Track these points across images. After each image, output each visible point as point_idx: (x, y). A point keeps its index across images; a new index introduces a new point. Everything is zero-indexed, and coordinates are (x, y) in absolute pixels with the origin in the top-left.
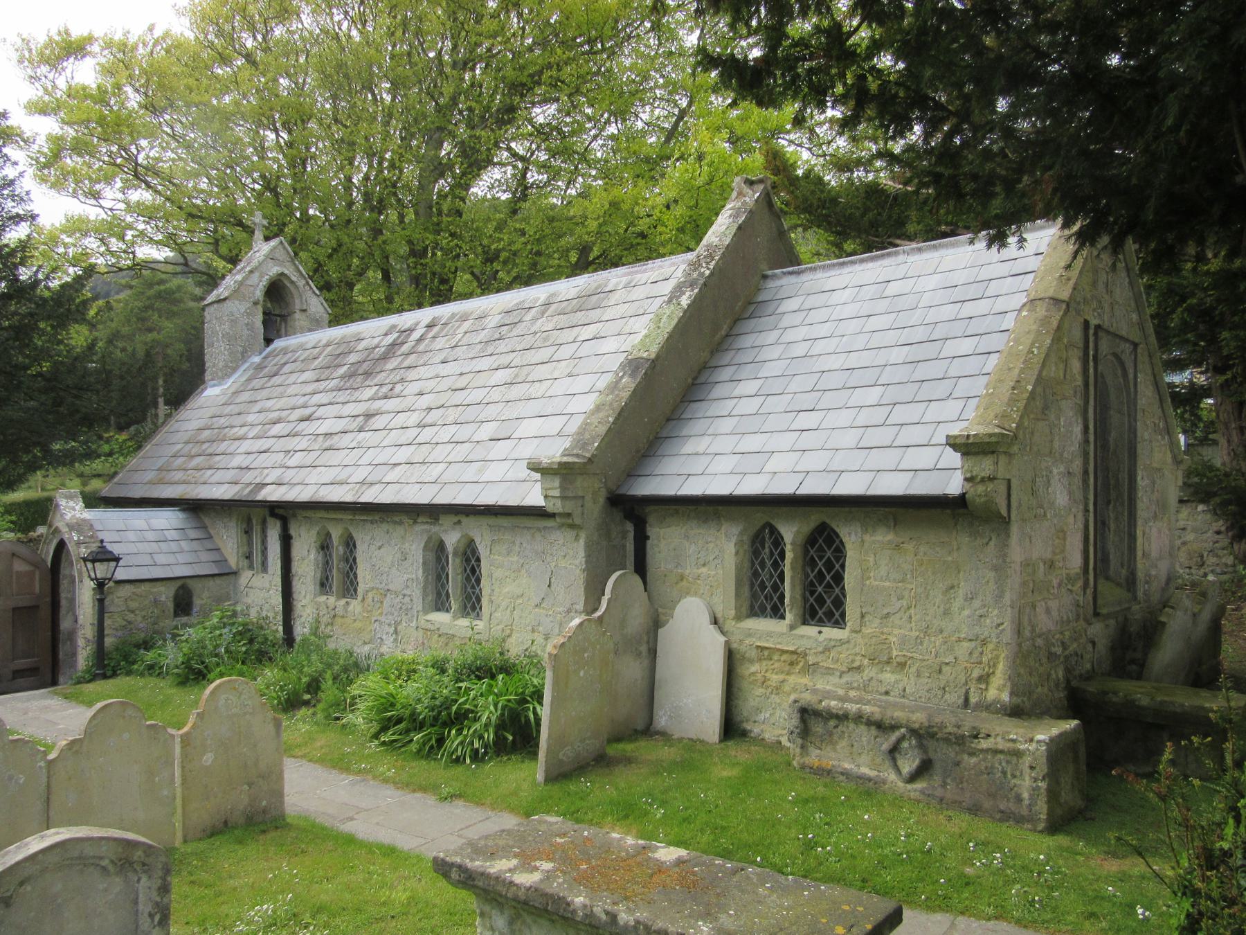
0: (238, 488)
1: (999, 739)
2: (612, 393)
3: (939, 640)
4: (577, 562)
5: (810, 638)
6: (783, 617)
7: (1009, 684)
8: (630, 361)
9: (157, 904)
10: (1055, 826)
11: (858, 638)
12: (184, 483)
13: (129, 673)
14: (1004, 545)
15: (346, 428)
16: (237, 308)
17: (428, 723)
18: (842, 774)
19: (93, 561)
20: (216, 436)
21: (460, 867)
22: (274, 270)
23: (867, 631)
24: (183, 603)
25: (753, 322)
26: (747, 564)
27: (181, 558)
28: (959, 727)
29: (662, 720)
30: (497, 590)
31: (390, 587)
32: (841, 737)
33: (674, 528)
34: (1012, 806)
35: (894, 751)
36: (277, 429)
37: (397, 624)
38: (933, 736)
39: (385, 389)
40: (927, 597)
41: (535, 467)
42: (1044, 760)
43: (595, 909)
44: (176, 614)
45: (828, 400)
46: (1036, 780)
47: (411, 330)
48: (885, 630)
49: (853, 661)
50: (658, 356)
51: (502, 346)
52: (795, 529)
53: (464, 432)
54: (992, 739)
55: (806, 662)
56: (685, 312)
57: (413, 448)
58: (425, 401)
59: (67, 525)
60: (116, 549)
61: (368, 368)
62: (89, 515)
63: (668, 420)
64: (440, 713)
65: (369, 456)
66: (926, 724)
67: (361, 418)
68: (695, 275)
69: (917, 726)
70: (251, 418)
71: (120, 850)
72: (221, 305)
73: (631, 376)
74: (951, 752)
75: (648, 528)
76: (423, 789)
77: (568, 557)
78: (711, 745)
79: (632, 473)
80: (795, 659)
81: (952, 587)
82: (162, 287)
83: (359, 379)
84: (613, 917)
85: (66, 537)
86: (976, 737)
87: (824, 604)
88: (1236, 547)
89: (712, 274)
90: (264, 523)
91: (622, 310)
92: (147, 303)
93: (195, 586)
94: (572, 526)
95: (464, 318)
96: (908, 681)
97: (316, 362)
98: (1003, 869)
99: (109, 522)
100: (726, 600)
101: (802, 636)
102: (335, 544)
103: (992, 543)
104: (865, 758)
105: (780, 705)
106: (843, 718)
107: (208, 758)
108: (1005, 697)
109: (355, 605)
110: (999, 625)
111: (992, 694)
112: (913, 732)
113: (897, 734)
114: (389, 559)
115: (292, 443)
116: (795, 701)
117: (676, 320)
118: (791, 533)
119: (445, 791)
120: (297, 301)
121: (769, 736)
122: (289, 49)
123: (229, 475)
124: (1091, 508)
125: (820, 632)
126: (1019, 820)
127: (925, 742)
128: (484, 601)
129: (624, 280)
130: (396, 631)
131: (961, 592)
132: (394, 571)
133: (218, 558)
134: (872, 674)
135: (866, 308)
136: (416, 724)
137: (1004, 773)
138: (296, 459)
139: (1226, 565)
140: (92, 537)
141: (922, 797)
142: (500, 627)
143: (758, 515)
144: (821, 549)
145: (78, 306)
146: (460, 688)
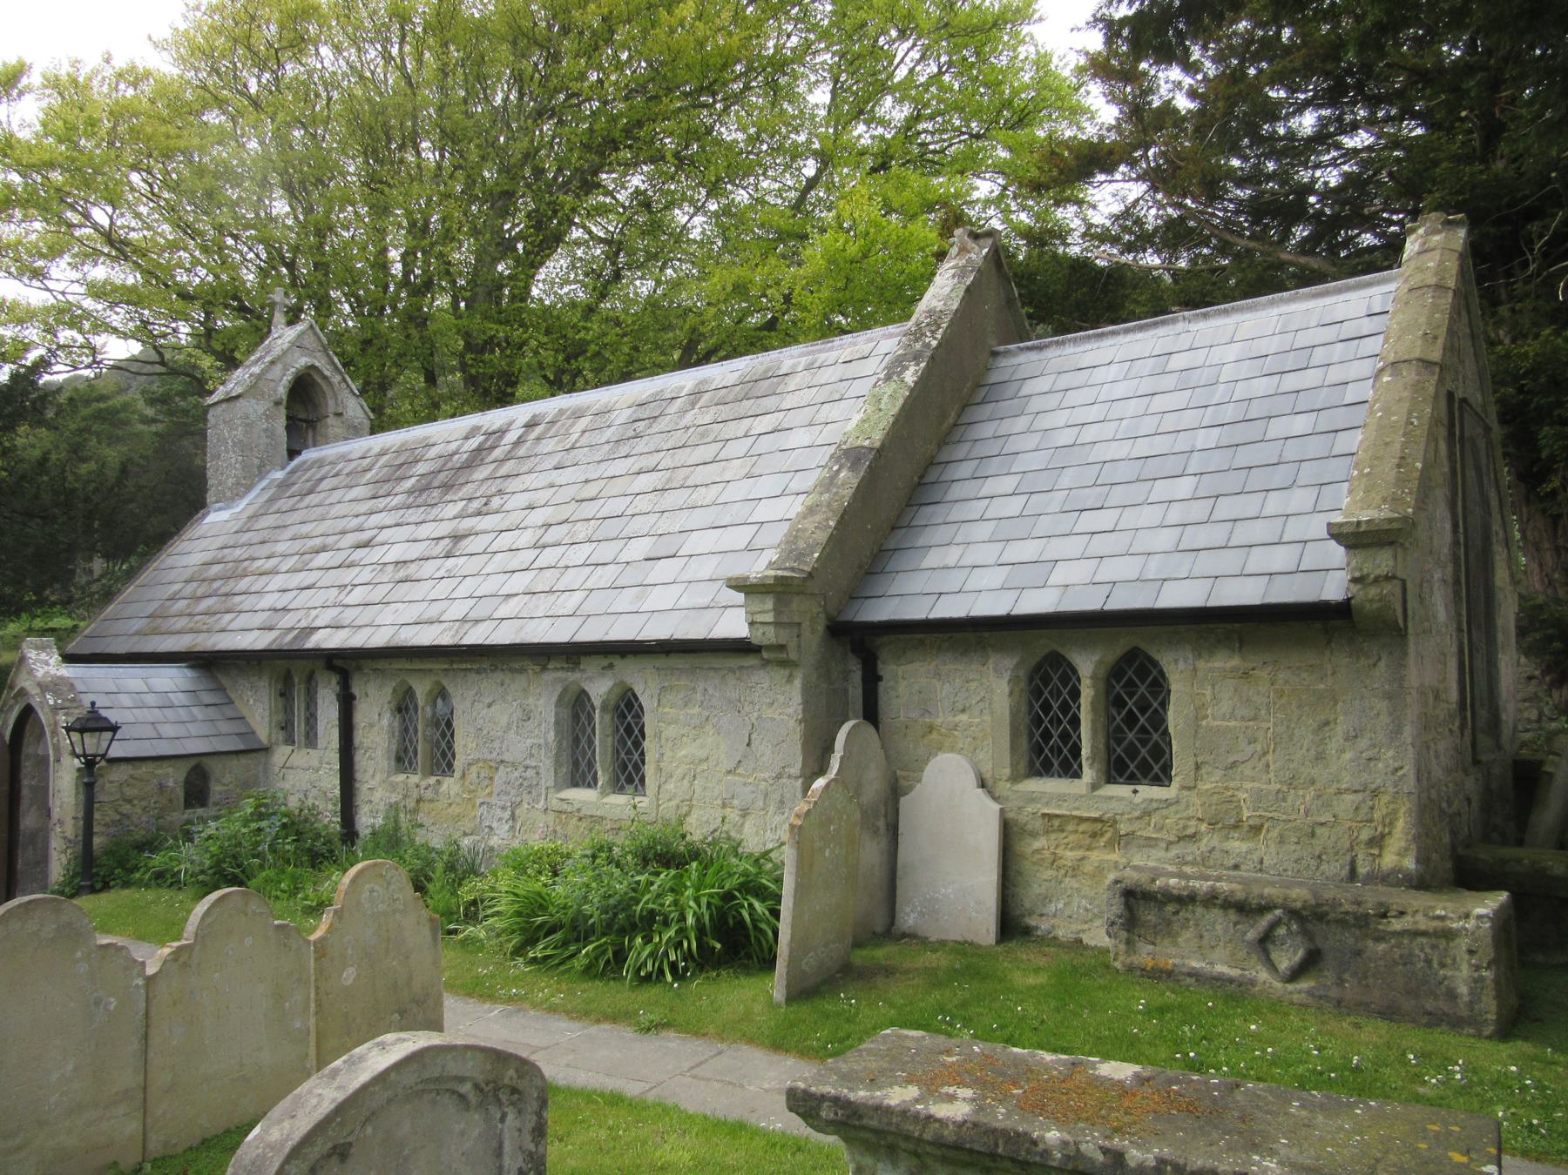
0: (273, 635)
1: (1419, 917)
2: (828, 491)
3: (1310, 793)
4: (791, 711)
5: (1122, 799)
6: (1077, 775)
7: (1413, 846)
8: (847, 452)
9: (531, 1154)
10: (1507, 1030)
11: (1194, 798)
12: (192, 631)
13: (126, 884)
14: (1400, 665)
15: (427, 554)
16: (255, 408)
17: (599, 930)
18: (1189, 975)
19: (82, 731)
20: (228, 574)
21: (836, 1101)
22: (303, 361)
23: (1205, 786)
24: (197, 790)
25: (989, 408)
26: (1024, 708)
27: (193, 729)
28: (1359, 904)
29: (909, 918)
30: (668, 754)
31: (506, 757)
32: (1185, 926)
33: (917, 665)
34: (1443, 1005)
35: (1265, 941)
36: (322, 559)
37: (515, 806)
38: (1321, 917)
39: (475, 505)
40: (1291, 737)
41: (739, 585)
42: (1489, 940)
43: (1083, 1147)
44: (188, 804)
45: (1118, 495)
46: (1477, 968)
47: (502, 432)
48: (1232, 785)
49: (1185, 827)
50: (883, 445)
51: (641, 446)
52: (1096, 658)
53: (605, 552)
54: (1408, 918)
55: (1117, 831)
56: (912, 390)
57: (531, 574)
58: (538, 517)
59: (39, 684)
60: (113, 716)
61: (447, 479)
62: (67, 671)
63: (893, 528)
64: (615, 915)
65: (467, 587)
66: (1313, 902)
67: (447, 541)
68: (918, 346)
69: (1299, 905)
70: (281, 548)
71: (489, 1067)
72: (231, 405)
73: (851, 469)
74: (1349, 938)
75: (880, 666)
76: (614, 1019)
77: (778, 705)
78: (986, 947)
79: (855, 595)
80: (1100, 829)
81: (1327, 723)
82: (102, 405)
83: (436, 493)
84: (1117, 1157)
85: (36, 701)
86: (1384, 916)
87: (1139, 754)
88: (1555, 694)
89: (940, 345)
90: (310, 678)
91: (807, 396)
92: (83, 424)
93: (215, 767)
94: (783, 664)
95: (578, 414)
96: (1266, 850)
97: (369, 475)
98: (1471, 1084)
99: (96, 681)
100: (997, 752)
101: (1111, 798)
102: (421, 703)
103: (1382, 664)
104: (1220, 953)
105: (1078, 890)
106: (1187, 900)
107: (349, 975)
108: (1410, 864)
109: (450, 785)
110: (1396, 770)
111: (1389, 860)
112: (1294, 914)
113: (1269, 917)
114: (504, 720)
115: (347, 576)
116: (1117, 882)
117: (901, 402)
118: (1087, 665)
119: (645, 1017)
120: (331, 402)
121: (1064, 932)
122: (305, 91)
123: (259, 619)
124: (1465, 627)
125: (1135, 792)
126: (1457, 1023)
127: (1309, 926)
128: (649, 770)
129: (804, 361)
130: (513, 817)
131: (1340, 730)
132: (511, 734)
133: (243, 730)
134: (1215, 842)
135: (1146, 386)
136: (578, 931)
137: (1428, 962)
138: (357, 596)
139: (1529, 721)
140: (73, 700)
141: (1310, 1000)
142: (673, 803)
143: (1039, 646)
144: (1130, 684)
145: (34, 402)
146: (638, 883)
